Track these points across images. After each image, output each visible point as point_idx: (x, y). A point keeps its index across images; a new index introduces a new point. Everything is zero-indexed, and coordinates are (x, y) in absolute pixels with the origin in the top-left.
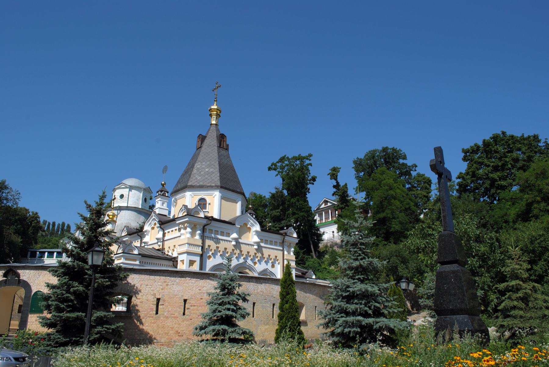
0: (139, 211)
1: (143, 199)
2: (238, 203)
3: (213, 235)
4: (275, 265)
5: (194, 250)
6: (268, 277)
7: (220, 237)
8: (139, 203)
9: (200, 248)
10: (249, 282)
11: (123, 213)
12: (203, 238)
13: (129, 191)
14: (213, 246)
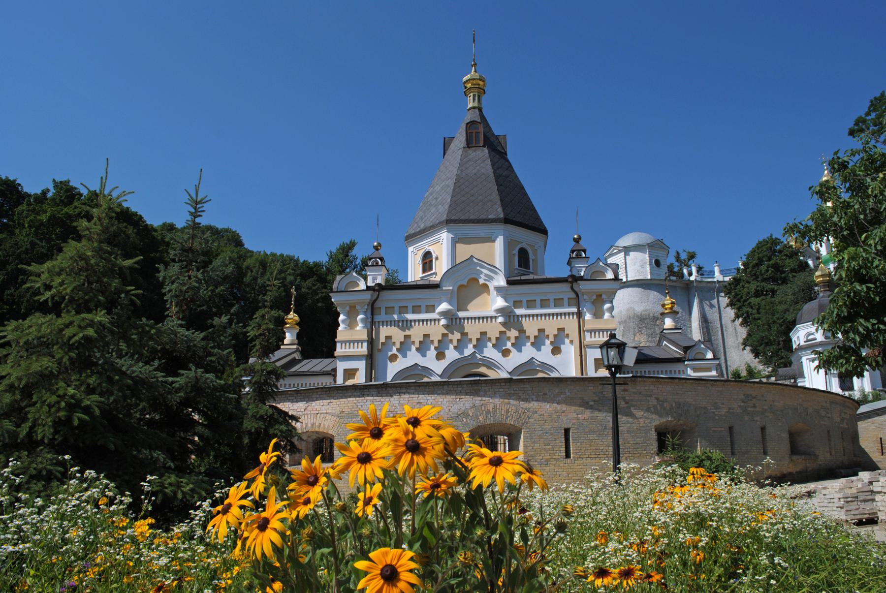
3: (396, 317)
4: (562, 347)
6: (540, 375)
7: (410, 316)
8: (646, 271)
9: (365, 344)
10: (363, 396)
12: (372, 325)
13: (625, 255)
14: (397, 335)
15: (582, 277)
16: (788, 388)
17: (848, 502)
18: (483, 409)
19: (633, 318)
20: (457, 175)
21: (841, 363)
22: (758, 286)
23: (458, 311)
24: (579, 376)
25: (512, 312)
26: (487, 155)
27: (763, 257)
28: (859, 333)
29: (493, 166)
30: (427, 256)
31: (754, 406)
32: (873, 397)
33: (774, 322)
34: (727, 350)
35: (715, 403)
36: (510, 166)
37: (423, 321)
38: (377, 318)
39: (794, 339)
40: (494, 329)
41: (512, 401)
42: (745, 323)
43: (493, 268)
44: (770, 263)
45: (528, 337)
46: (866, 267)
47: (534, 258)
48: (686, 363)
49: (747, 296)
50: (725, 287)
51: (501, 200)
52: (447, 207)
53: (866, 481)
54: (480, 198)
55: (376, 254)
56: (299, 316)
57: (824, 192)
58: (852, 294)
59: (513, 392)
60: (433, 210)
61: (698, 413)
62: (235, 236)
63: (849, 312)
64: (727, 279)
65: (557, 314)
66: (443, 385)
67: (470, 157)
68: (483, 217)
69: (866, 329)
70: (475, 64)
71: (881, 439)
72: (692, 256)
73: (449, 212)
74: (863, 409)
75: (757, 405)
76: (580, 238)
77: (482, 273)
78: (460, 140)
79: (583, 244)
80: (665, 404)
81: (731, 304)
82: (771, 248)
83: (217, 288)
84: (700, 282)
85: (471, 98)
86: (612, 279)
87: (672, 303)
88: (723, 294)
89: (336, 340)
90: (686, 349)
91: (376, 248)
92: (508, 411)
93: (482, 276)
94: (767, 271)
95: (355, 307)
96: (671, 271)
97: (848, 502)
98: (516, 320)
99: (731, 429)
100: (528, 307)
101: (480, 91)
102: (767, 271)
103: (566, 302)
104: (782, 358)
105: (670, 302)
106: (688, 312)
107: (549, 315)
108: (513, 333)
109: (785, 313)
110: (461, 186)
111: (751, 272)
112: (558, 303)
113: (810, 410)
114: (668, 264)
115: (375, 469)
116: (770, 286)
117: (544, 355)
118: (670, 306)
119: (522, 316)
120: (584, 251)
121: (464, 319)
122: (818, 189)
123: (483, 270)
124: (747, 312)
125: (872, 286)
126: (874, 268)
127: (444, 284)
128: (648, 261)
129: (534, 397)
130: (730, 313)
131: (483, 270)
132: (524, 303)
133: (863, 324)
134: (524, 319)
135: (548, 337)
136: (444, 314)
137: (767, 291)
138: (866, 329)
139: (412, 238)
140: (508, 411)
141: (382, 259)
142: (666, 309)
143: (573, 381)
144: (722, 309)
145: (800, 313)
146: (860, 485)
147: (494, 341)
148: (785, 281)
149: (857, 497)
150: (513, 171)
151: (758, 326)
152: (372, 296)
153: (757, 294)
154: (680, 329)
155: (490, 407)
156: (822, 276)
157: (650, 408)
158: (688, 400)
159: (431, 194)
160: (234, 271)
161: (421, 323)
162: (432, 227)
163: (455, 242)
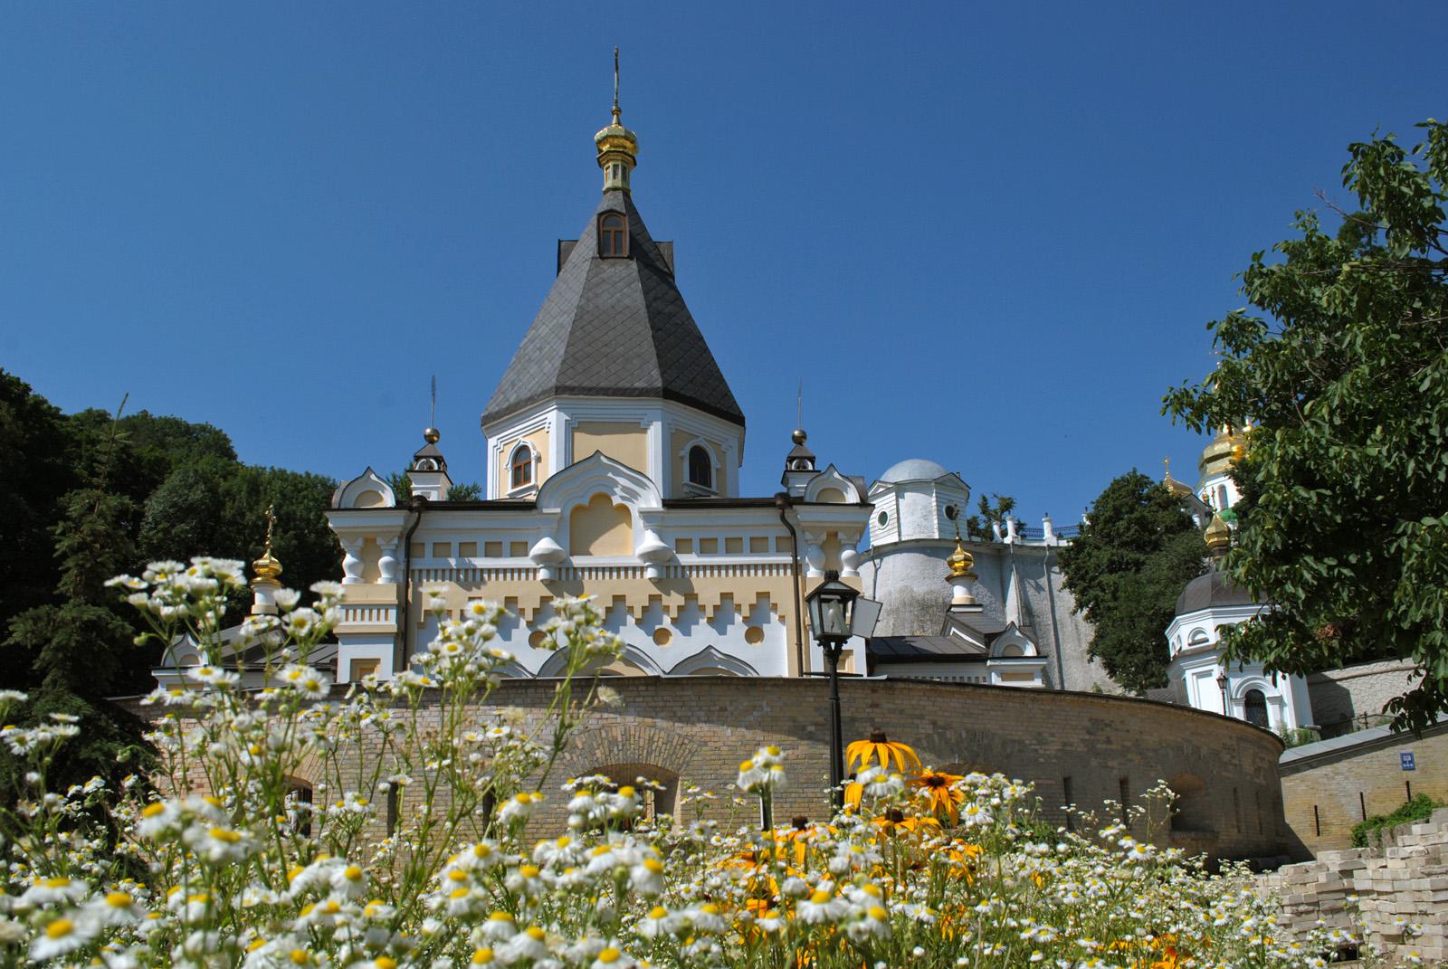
0: (931, 548)
1: (939, 511)
2: (649, 431)
4: (765, 627)
5: (351, 622)
7: (481, 562)
8: (932, 526)
9: (393, 613)
11: (892, 563)
12: (407, 576)
13: (897, 497)
15: (802, 498)
16: (1167, 709)
17: (1299, 914)
18: (604, 735)
19: (911, 605)
20: (579, 307)
21: (1269, 646)
22: (1113, 555)
23: (572, 554)
24: (796, 675)
25: (673, 559)
26: (635, 274)
27: (1122, 506)
28: (1304, 584)
29: (646, 293)
30: (522, 451)
31: (1109, 741)
32: (1300, 739)
33: (1141, 615)
34: (1063, 663)
35: (1039, 734)
36: (678, 298)
37: (505, 571)
38: (417, 564)
39: (1172, 640)
40: (639, 591)
41: (659, 722)
42: (1093, 616)
43: (639, 476)
44: (1133, 516)
45: (703, 608)
46: (1316, 456)
47: (719, 466)
48: (989, 663)
49: (1096, 570)
50: (1061, 554)
51: (658, 356)
52: (558, 363)
53: (1335, 869)
54: (621, 349)
55: (430, 450)
56: (281, 561)
57: (1237, 333)
58: (1290, 507)
59: (661, 704)
60: (534, 369)
61: (1009, 751)
62: (219, 439)
63: (1284, 544)
64: (1063, 543)
65: (756, 567)
66: (526, 688)
67: (604, 276)
68: (625, 384)
69: (1317, 575)
70: (618, 111)
71: (1316, 807)
72: (1007, 506)
73: (562, 373)
74: (1287, 756)
75: (1112, 739)
76: (803, 436)
77: (616, 484)
78: (587, 245)
79: (810, 447)
80: (948, 734)
81: (1070, 585)
82: (1134, 492)
83: (173, 526)
84: (1021, 547)
85: (610, 170)
86: (856, 504)
87: (966, 559)
88: (1056, 569)
90: (989, 638)
91: (430, 439)
92: (651, 740)
93: (617, 490)
94: (1128, 529)
95: (374, 540)
96: (974, 529)
97: (1299, 914)
98: (679, 575)
99: (1067, 780)
100: (703, 552)
101: (627, 161)
102: (1128, 529)
103: (772, 543)
104: (1152, 675)
105: (962, 557)
106: (1000, 599)
107: (741, 567)
108: (675, 600)
109: (1157, 600)
110: (586, 325)
111: (1102, 530)
112: (757, 546)
113: (1204, 751)
114: (969, 518)
115: (117, 809)
116: (1132, 555)
117: (732, 643)
118: (962, 564)
119: (691, 568)
120: (812, 460)
121: (583, 569)
122: (1224, 326)
123: (618, 479)
124: (1096, 598)
125: (1328, 492)
126: (1331, 459)
127: (543, 502)
128: (935, 508)
129: (702, 714)
130: (1068, 599)
131: (618, 479)
132: (696, 544)
133: (1312, 567)
134: (694, 573)
135: (738, 608)
136: (544, 559)
137: (1128, 563)
138: (1317, 575)
139: (496, 420)
140: (651, 740)
141: (439, 460)
142: (956, 570)
143: (775, 685)
144: (1055, 593)
145: (1180, 598)
146: (1322, 878)
147: (638, 614)
148: (1156, 546)
149: (1317, 904)
150: (684, 307)
151: (1114, 621)
152: (406, 521)
153: (1113, 567)
154: (980, 606)
155: (617, 732)
156: (1217, 534)
157: (919, 740)
158: (988, 726)
159: (532, 341)
160: (204, 497)
161: (501, 576)
162: (531, 400)
163: (571, 429)
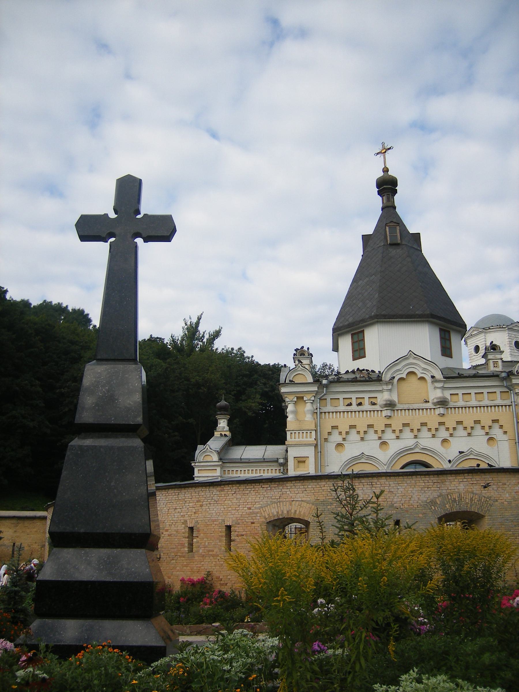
18: (450, 497)
89: (286, 430)
92: (471, 499)
